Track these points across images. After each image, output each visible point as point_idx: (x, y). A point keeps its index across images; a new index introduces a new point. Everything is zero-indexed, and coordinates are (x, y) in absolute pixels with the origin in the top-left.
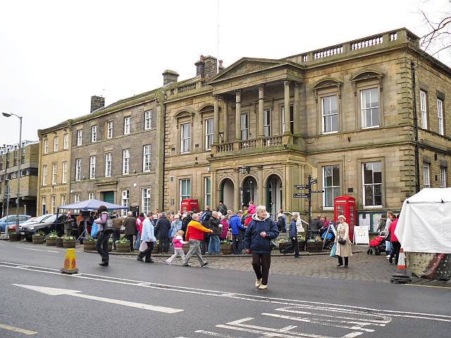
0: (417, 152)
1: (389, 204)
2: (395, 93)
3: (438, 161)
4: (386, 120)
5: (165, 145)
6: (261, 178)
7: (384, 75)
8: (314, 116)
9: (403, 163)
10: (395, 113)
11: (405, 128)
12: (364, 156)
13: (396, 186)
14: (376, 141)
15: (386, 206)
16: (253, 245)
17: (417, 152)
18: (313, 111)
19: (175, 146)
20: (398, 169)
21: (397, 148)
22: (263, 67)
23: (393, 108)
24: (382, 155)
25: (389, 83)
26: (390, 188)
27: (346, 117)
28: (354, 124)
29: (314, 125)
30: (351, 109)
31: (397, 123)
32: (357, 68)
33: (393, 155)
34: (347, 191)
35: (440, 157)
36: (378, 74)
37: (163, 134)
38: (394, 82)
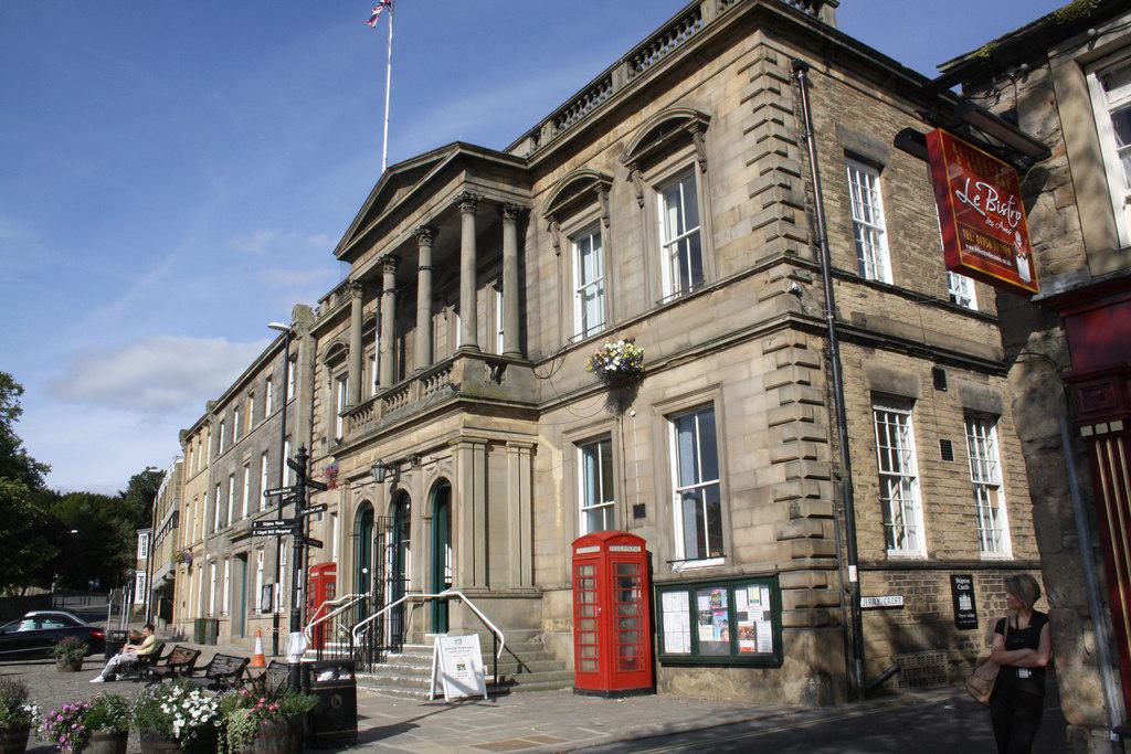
0: (831, 356)
1: (744, 554)
2: (740, 163)
3: (950, 392)
4: (721, 261)
5: (312, 434)
6: (418, 484)
7: (708, 118)
8: (554, 295)
9: (775, 396)
10: (744, 229)
11: (775, 272)
12: (671, 393)
13: (761, 482)
14: (697, 337)
15: (735, 560)
16: (1088, 641)
17: (831, 356)
18: (553, 280)
20: (762, 422)
21: (754, 347)
22: (413, 183)
23: (737, 214)
24: (714, 379)
25: (722, 141)
26: (741, 494)
27: (624, 277)
28: (639, 295)
29: (554, 319)
30: (634, 251)
31: (750, 262)
32: (630, 130)
33: (746, 376)
34: (631, 515)
35: (955, 377)
36: (685, 120)
37: (309, 408)
38: (735, 133)
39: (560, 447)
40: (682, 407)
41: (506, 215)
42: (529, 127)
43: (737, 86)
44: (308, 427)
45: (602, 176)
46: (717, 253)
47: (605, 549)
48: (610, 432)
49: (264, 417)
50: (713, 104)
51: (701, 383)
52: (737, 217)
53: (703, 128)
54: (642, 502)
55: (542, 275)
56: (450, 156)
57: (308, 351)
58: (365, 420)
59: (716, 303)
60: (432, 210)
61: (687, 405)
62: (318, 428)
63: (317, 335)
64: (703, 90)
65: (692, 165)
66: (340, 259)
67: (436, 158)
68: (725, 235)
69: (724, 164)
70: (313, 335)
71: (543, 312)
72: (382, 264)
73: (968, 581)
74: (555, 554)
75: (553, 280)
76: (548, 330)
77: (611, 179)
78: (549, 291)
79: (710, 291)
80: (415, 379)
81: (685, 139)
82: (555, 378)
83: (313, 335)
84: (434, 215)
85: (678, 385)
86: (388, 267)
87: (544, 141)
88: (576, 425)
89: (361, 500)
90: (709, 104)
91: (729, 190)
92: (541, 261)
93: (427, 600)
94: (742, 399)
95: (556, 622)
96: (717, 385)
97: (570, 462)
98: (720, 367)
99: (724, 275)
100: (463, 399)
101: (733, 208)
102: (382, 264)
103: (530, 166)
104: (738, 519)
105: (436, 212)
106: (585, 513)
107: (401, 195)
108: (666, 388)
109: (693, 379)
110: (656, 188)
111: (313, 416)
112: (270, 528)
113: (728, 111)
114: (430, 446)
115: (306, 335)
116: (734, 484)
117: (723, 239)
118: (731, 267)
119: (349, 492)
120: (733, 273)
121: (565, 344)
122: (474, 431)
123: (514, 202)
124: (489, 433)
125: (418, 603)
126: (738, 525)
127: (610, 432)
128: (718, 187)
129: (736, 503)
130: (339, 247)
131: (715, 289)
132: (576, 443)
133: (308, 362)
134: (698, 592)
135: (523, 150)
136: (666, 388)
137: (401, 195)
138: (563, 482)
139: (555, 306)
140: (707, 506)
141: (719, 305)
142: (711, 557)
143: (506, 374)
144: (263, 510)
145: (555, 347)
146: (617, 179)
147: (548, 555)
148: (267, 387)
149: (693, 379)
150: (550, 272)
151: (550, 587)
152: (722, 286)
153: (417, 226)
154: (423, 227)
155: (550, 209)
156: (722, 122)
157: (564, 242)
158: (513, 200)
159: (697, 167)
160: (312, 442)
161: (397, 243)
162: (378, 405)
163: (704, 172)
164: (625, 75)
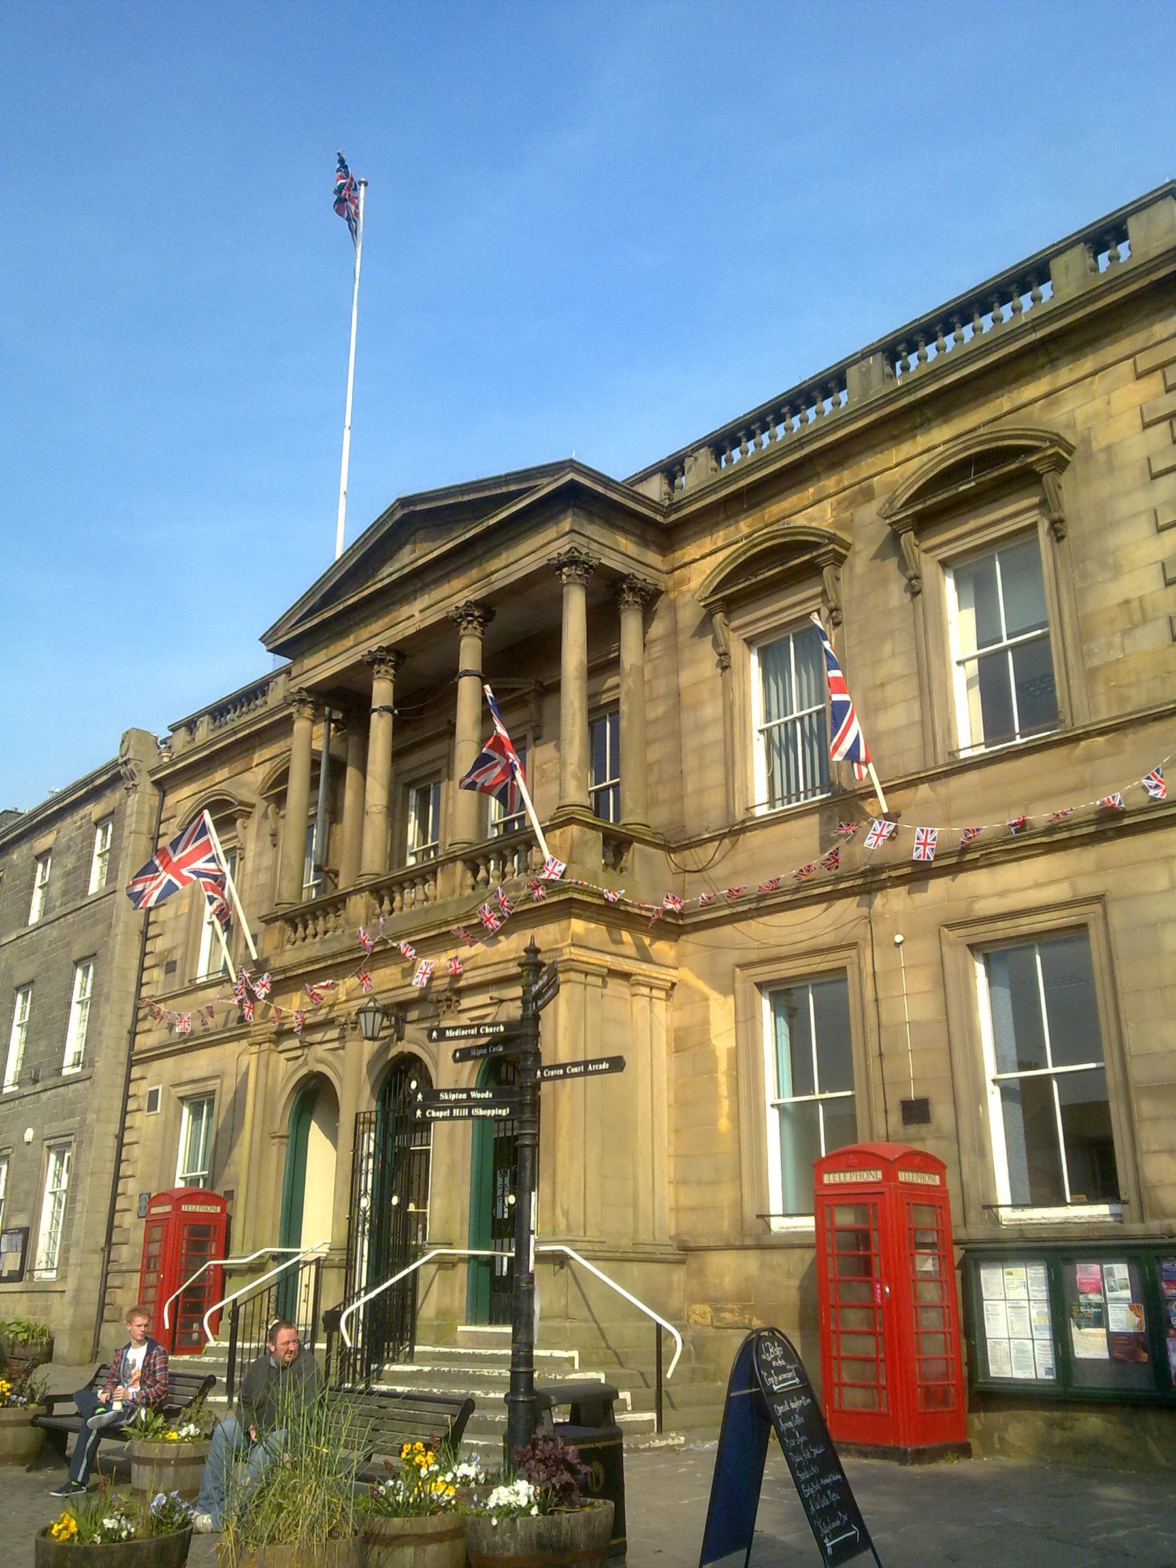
4: (1101, 688)
5: (144, 954)
7: (1070, 450)
15: (1145, 1207)
18: (711, 710)
19: (177, 955)
24: (1088, 887)
25: (1102, 488)
28: (912, 740)
29: (715, 775)
34: (895, 1117)
38: (1131, 475)
39: (728, 990)
40: (1011, 933)
41: (629, 597)
42: (663, 452)
43: (1136, 399)
44: (137, 940)
45: (833, 539)
46: (1091, 675)
47: (890, 1176)
48: (844, 968)
49: (26, 924)
50: (1079, 428)
51: (1058, 893)
52: (1137, 617)
53: (1060, 464)
54: (923, 1094)
55: (686, 699)
56: (548, 487)
57: (147, 809)
58: (321, 927)
59: (1089, 758)
60: (494, 577)
61: (1025, 930)
62: (157, 946)
63: (163, 786)
64: (1056, 403)
65: (1033, 527)
66: (269, 651)
67: (513, 488)
68: (1110, 646)
69: (1107, 525)
70: (157, 783)
71: (690, 762)
72: (371, 664)
73: (153, 1260)
74: (714, 1183)
75: (711, 710)
76: (700, 791)
77: (847, 547)
78: (700, 728)
79: (1077, 739)
80: (453, 859)
81: (1027, 479)
82: (718, 872)
83: (157, 783)
84: (498, 586)
85: (1003, 894)
86: (383, 668)
87: (688, 482)
88: (764, 954)
89: (303, 1071)
90: (1071, 425)
91: (1116, 571)
92: (685, 678)
93: (462, 1259)
94: (1154, 926)
95: (721, 1310)
96: (1099, 898)
97: (747, 1022)
98: (1101, 868)
99: (1106, 713)
100: (576, 896)
101: (1127, 602)
102: (371, 664)
103: (674, 517)
104: (1148, 1136)
105: (501, 580)
106: (776, 1112)
107: (409, 558)
108: (978, 898)
109: (1038, 885)
110: (944, 564)
111: (148, 924)
112: (458, 1104)
113: (1115, 440)
114: (490, 977)
115: (145, 782)
116: (1139, 1072)
117: (1104, 650)
118: (1123, 700)
119: (274, 1056)
120: (1129, 709)
121: (739, 815)
122: (588, 953)
123: (642, 577)
124: (608, 958)
125: (443, 1263)
126: (1154, 1147)
127: (844, 968)
128: (1090, 566)
129: (1145, 1107)
130: (275, 629)
131: (1088, 735)
132: (760, 986)
133: (144, 828)
134: (982, 1265)
135: (655, 489)
136: (978, 898)
137: (409, 558)
138: (734, 1054)
139: (717, 753)
140: (1061, 1106)
141: (1098, 763)
142: (1072, 1204)
143: (627, 858)
144: (66, 1072)
145: (715, 820)
146: (858, 546)
147: (699, 1183)
148: (35, 870)
149: (1038, 885)
150: (706, 696)
151: (703, 1243)
152: (1102, 732)
153: (460, 600)
154: (469, 605)
155: (715, 591)
156: (1102, 457)
157: (736, 648)
158: (641, 573)
159: (1043, 527)
160: (142, 969)
161: (408, 629)
162: (358, 905)
163: (1060, 539)
164: (876, 376)
